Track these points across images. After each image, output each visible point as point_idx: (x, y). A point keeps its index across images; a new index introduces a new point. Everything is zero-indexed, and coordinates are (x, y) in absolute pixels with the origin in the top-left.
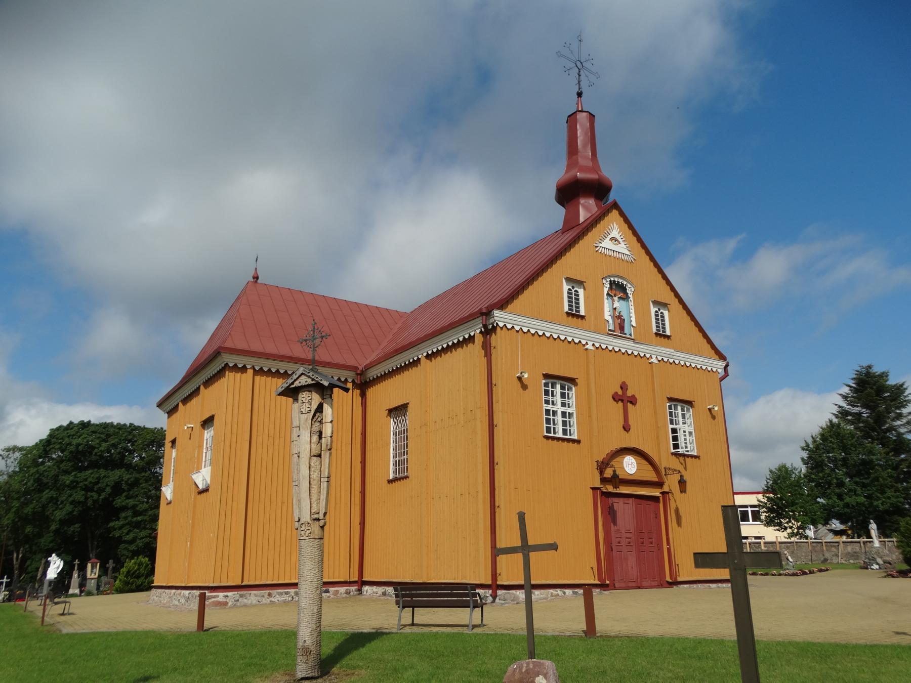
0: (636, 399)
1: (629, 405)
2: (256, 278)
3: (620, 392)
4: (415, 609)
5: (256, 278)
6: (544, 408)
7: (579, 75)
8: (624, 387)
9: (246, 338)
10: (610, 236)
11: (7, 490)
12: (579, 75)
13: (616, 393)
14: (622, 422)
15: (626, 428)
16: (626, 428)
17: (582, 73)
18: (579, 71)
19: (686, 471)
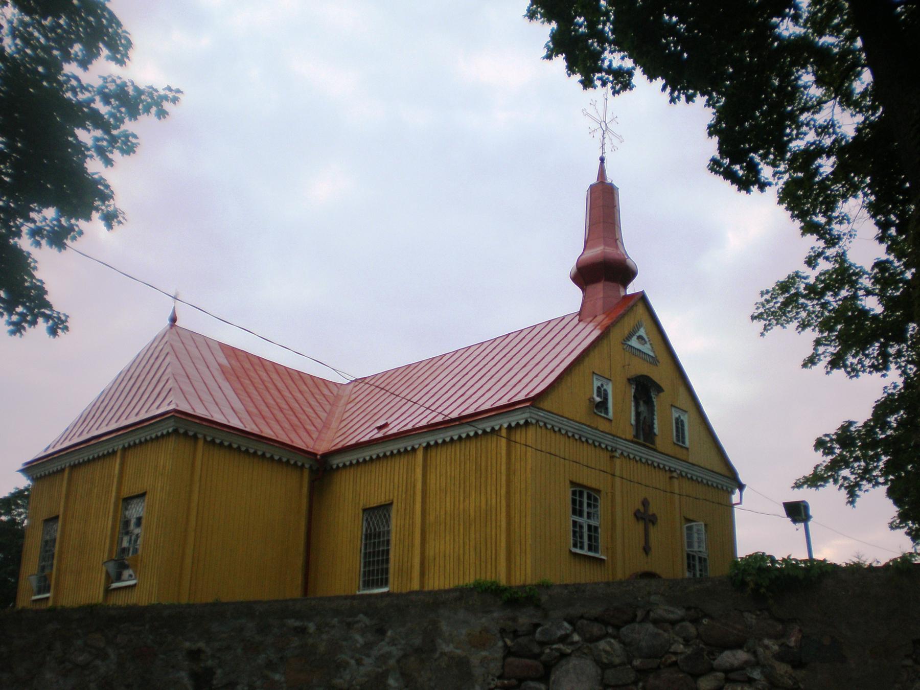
0: (656, 519)
1: (650, 525)
2: (174, 320)
3: (642, 509)
4: (294, 591)
5: (174, 320)
6: (572, 519)
7: (604, 138)
8: (645, 503)
9: (214, 399)
10: (637, 334)
11: (1, 499)
12: (604, 138)
13: (638, 510)
14: (643, 543)
15: (647, 550)
16: (647, 550)
17: (606, 135)
18: (604, 133)
19: (805, 365)
